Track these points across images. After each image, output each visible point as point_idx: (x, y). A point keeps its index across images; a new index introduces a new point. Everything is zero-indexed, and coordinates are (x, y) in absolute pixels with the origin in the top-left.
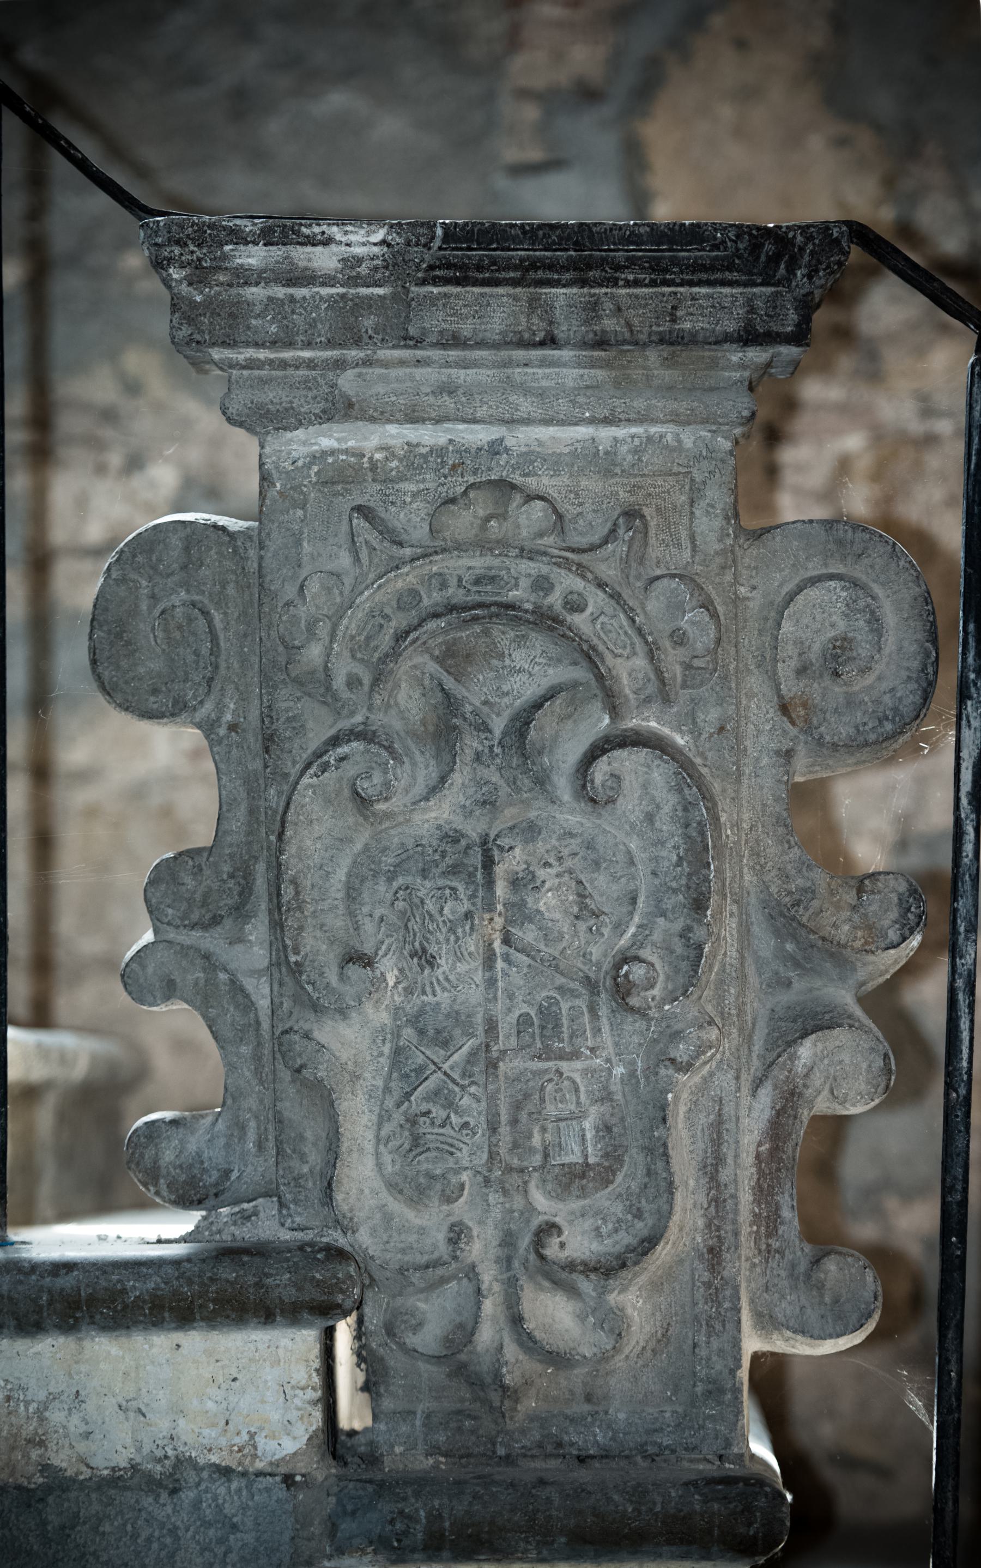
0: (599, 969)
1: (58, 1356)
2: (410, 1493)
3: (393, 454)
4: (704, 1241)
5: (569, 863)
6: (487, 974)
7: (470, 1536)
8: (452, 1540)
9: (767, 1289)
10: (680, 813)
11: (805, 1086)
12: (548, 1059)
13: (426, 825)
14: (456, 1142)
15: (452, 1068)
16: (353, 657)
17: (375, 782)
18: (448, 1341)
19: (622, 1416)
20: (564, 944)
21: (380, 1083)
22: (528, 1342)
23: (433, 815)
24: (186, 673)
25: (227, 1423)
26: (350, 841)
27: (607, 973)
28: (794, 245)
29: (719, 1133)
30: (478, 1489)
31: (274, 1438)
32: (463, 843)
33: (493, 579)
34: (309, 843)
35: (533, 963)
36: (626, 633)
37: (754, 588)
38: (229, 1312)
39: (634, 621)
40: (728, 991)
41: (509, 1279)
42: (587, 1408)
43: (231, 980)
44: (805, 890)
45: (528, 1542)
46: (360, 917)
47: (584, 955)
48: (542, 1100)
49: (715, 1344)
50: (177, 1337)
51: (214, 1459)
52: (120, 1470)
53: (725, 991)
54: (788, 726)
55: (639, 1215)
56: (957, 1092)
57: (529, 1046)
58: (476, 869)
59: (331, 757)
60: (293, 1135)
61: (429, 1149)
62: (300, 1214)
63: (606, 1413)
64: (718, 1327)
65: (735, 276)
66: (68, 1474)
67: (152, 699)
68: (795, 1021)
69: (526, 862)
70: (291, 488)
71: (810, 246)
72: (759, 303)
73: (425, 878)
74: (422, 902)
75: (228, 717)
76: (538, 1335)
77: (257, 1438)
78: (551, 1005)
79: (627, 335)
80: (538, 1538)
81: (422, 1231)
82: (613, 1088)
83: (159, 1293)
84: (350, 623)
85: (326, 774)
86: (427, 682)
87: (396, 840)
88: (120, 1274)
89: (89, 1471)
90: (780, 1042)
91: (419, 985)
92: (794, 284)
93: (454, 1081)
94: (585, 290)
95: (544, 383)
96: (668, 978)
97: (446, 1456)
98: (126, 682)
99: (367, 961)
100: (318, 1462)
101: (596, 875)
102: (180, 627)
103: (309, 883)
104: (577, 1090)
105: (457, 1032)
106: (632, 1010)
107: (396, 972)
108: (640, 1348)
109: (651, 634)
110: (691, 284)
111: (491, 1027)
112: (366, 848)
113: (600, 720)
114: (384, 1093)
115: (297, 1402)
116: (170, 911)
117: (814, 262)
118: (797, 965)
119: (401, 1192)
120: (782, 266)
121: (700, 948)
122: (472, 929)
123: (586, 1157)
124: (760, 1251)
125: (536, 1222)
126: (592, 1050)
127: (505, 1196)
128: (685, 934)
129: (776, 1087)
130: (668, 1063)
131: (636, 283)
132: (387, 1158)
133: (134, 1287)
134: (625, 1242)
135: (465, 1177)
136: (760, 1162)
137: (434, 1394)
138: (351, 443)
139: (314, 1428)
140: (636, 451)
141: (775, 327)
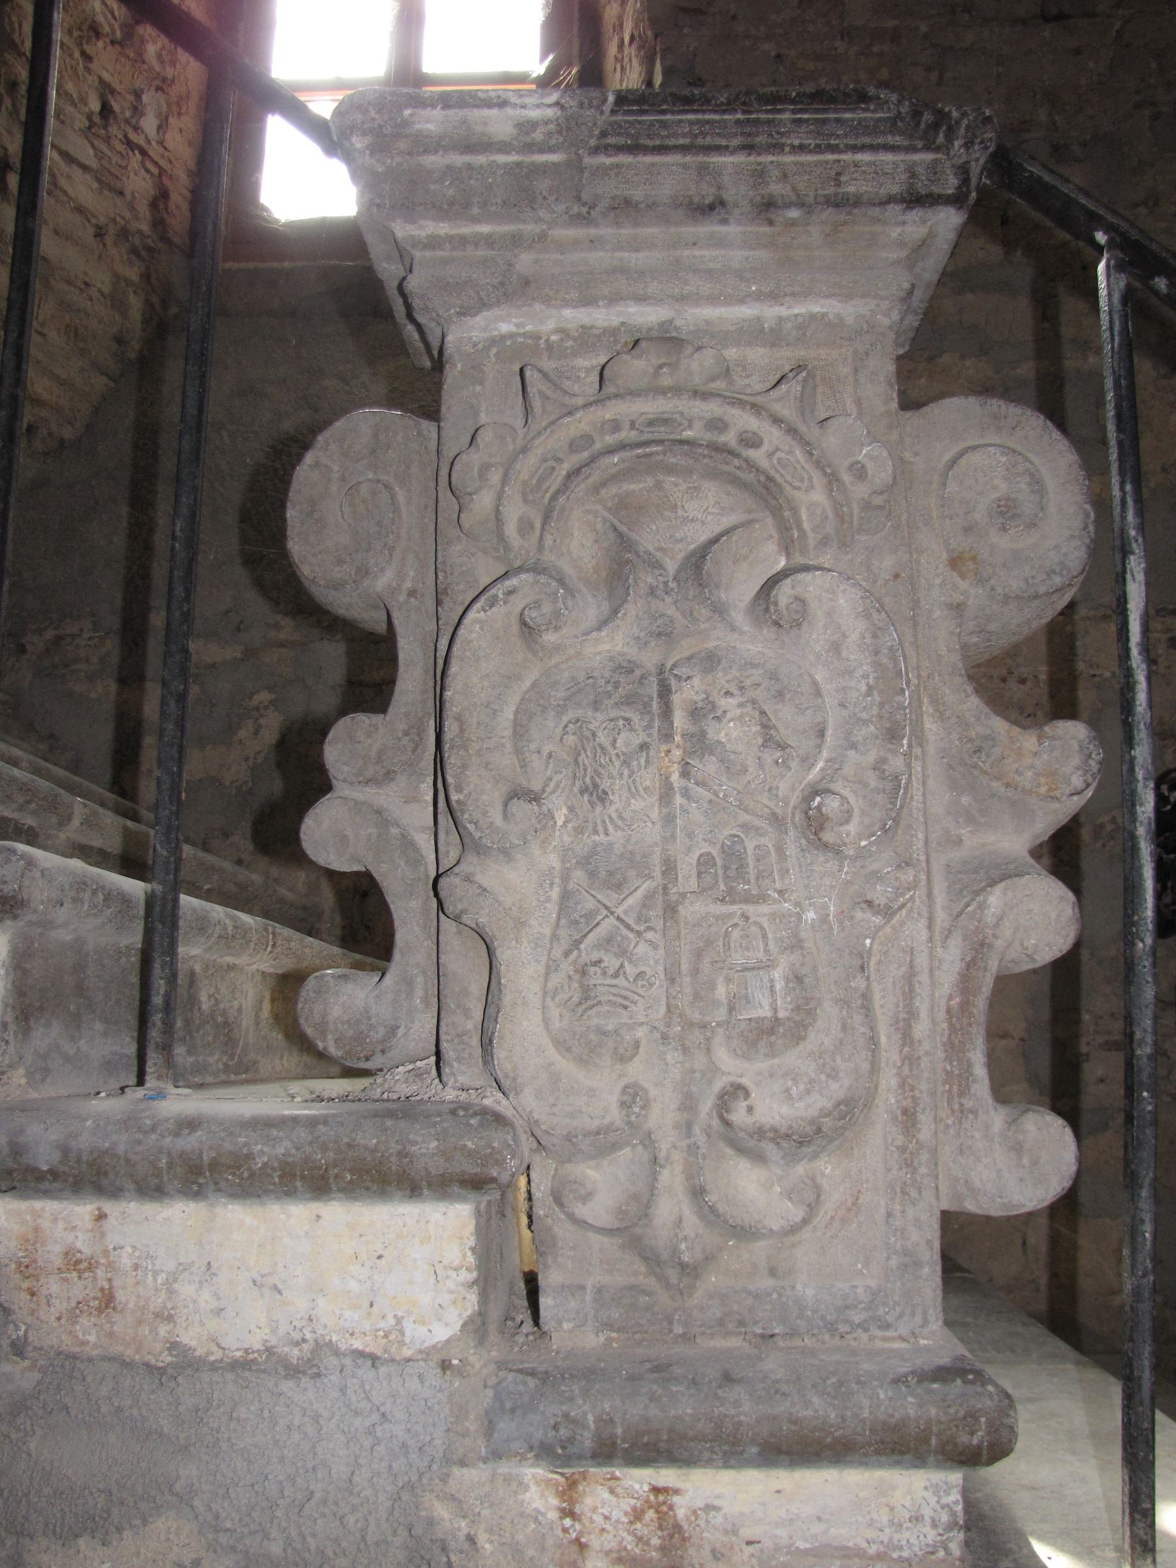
0: (787, 804)
1: (189, 1223)
2: (577, 1392)
3: (568, 335)
4: (898, 1101)
5: (751, 693)
6: (664, 810)
7: (647, 1444)
8: (626, 1449)
9: (961, 1152)
10: (868, 640)
11: (994, 936)
12: (733, 902)
13: (598, 658)
14: (630, 994)
15: (626, 912)
16: (525, 500)
17: (544, 611)
18: (620, 1212)
19: (810, 1292)
20: (749, 777)
21: (547, 931)
22: (711, 1215)
23: (606, 647)
24: (369, 544)
25: (371, 1305)
26: (519, 678)
27: (795, 808)
28: (950, 118)
29: (911, 986)
30: (655, 1387)
31: (423, 1323)
32: (638, 673)
33: (666, 421)
34: (475, 680)
35: (713, 798)
36: (803, 467)
37: (917, 454)
38: (369, 1184)
39: (811, 454)
40: (916, 836)
41: (689, 1146)
42: (770, 1283)
43: (403, 835)
44: (986, 738)
45: (713, 1452)
46: (527, 755)
47: (770, 789)
48: (727, 946)
49: (911, 1213)
50: (316, 1207)
51: (358, 1344)
52: (253, 1352)
53: (912, 836)
54: (958, 580)
55: (833, 1075)
56: (1142, 941)
57: (711, 888)
58: (652, 699)
59: (499, 591)
60: (457, 989)
61: (599, 1003)
62: (464, 1073)
63: (793, 1288)
64: (914, 1194)
65: (897, 140)
66: (197, 1353)
67: (337, 569)
68: (976, 872)
69: (705, 692)
70: (472, 368)
71: (965, 122)
72: (920, 170)
73: (596, 710)
74: (594, 735)
75: (408, 584)
76: (721, 1208)
77: (404, 1323)
78: (734, 843)
79: (794, 198)
80: (726, 1448)
81: (592, 1092)
82: (804, 935)
83: (290, 1159)
84: (526, 468)
85: (494, 609)
86: (599, 526)
87: (566, 675)
88: (246, 1137)
89: (221, 1352)
90: (965, 892)
91: (590, 824)
92: (952, 153)
93: (628, 927)
94: (752, 158)
95: (711, 265)
96: (863, 813)
97: (619, 1330)
98: (314, 555)
99: (535, 798)
100: (476, 1347)
101: (780, 706)
102: (364, 501)
103: (474, 721)
104: (765, 936)
105: (632, 873)
106: (826, 846)
107: (565, 810)
108: (828, 1217)
109: (829, 466)
110: (855, 149)
111: (669, 867)
112: (535, 684)
113: (776, 562)
114: (551, 942)
115: (450, 1284)
116: (346, 768)
117: (969, 135)
118: (970, 820)
119: (569, 1050)
120: (941, 135)
121: (896, 778)
122: (647, 761)
123: (775, 1010)
124: (953, 1111)
125: (719, 1084)
126: (781, 892)
127: (684, 1054)
128: (878, 766)
129: (965, 938)
130: (864, 906)
131: (802, 148)
132: (555, 1013)
133: (262, 1151)
134: (819, 1105)
135: (640, 1033)
136: (951, 1018)
137: (605, 1267)
138: (529, 328)
139: (469, 1313)
140: (799, 327)
141: (936, 190)
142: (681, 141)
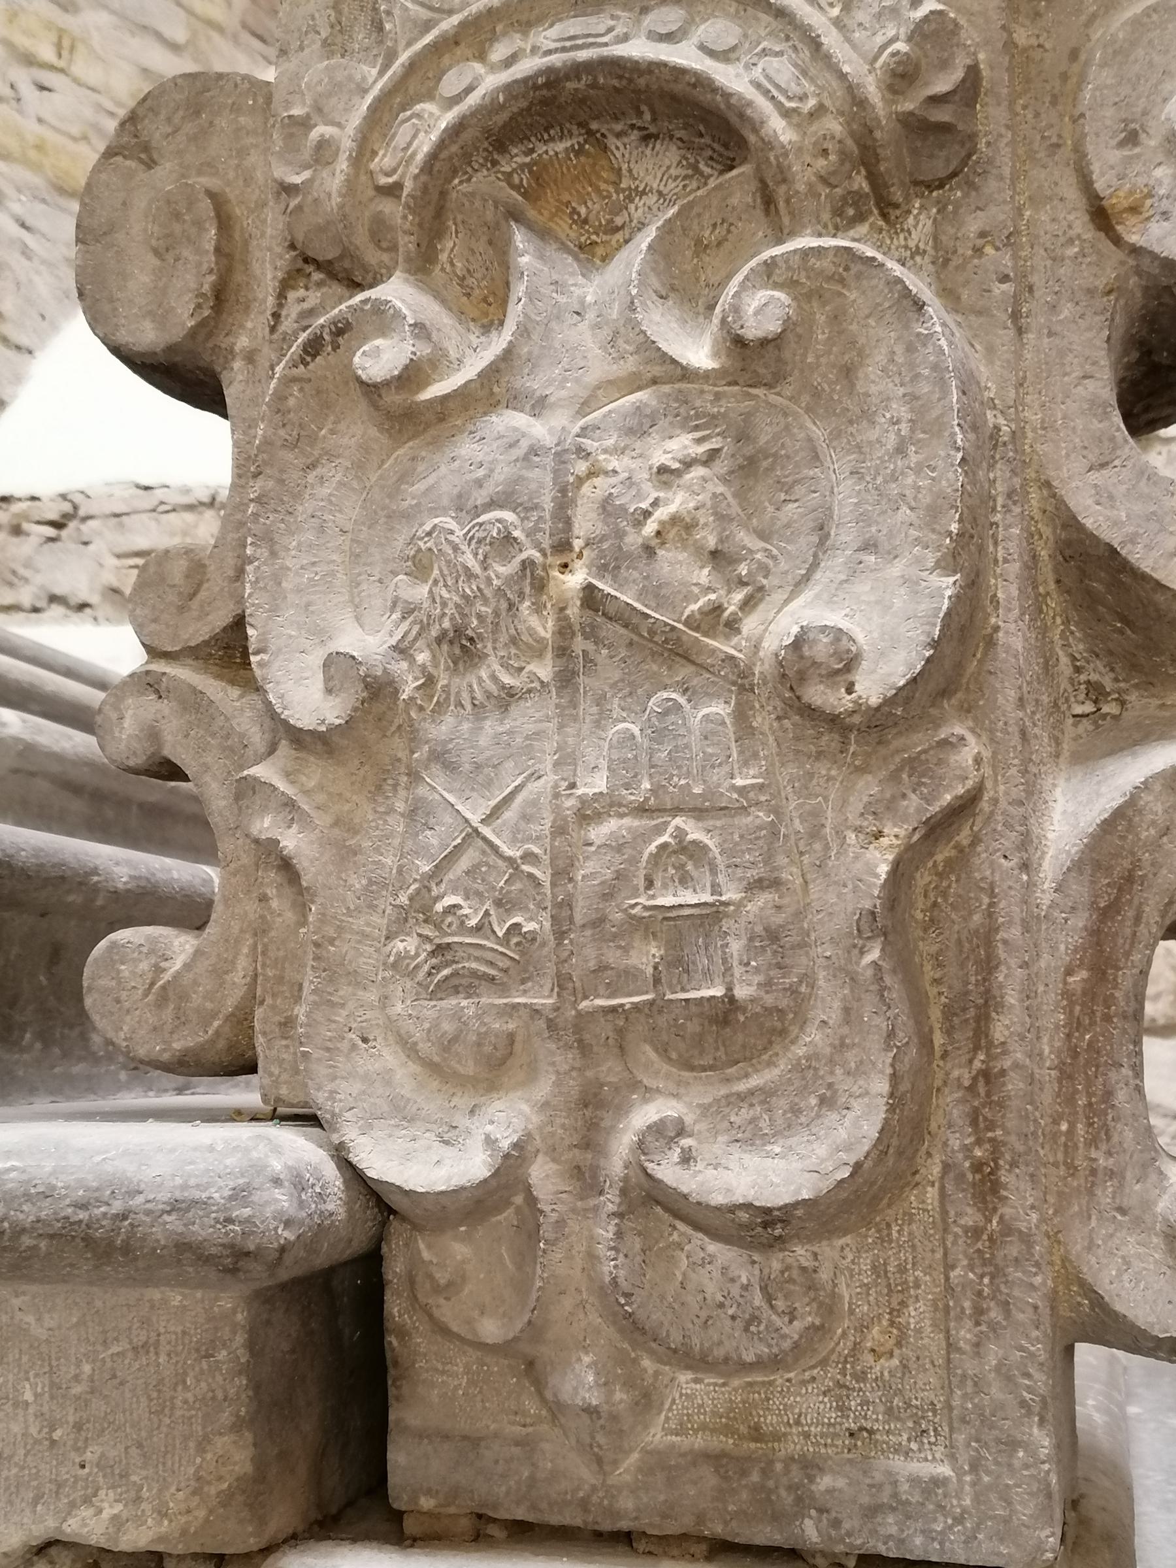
142: (414, 632)
